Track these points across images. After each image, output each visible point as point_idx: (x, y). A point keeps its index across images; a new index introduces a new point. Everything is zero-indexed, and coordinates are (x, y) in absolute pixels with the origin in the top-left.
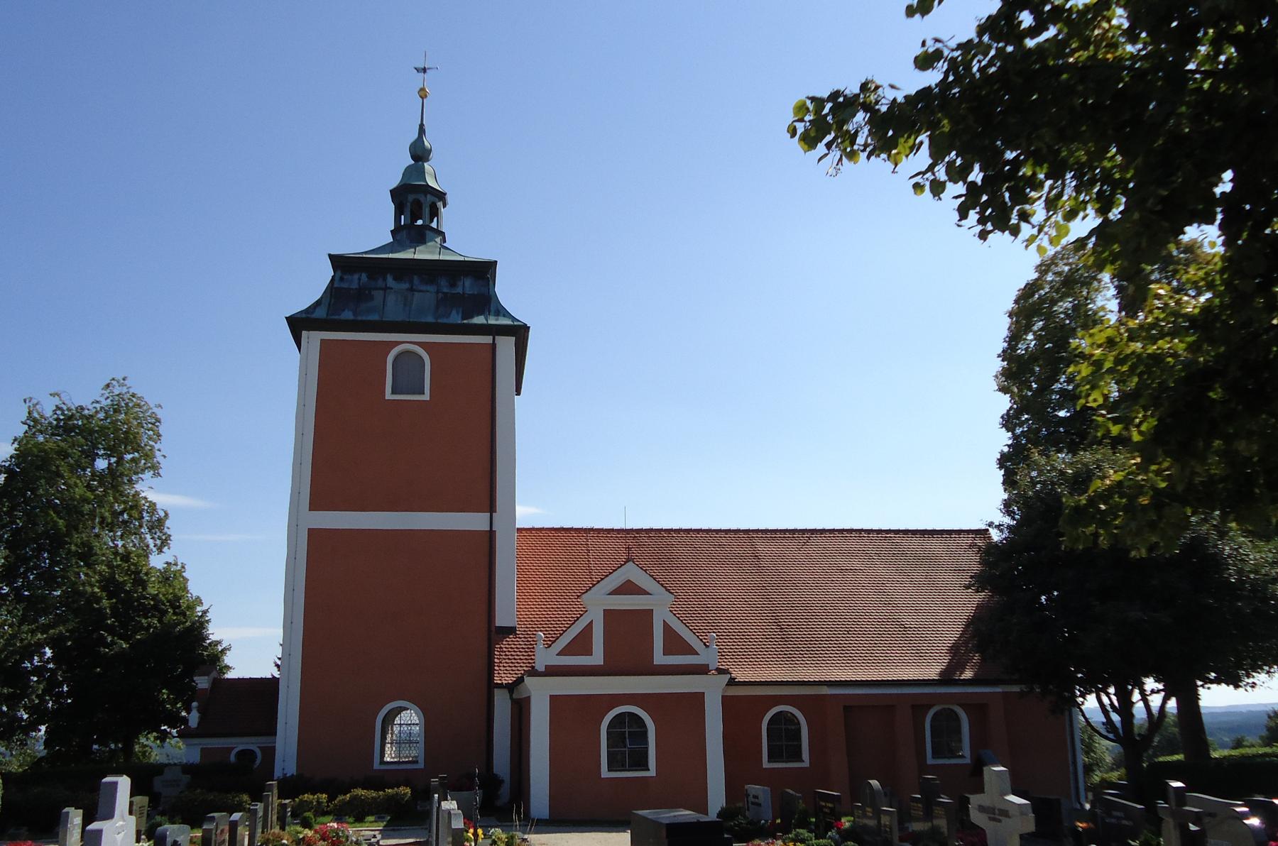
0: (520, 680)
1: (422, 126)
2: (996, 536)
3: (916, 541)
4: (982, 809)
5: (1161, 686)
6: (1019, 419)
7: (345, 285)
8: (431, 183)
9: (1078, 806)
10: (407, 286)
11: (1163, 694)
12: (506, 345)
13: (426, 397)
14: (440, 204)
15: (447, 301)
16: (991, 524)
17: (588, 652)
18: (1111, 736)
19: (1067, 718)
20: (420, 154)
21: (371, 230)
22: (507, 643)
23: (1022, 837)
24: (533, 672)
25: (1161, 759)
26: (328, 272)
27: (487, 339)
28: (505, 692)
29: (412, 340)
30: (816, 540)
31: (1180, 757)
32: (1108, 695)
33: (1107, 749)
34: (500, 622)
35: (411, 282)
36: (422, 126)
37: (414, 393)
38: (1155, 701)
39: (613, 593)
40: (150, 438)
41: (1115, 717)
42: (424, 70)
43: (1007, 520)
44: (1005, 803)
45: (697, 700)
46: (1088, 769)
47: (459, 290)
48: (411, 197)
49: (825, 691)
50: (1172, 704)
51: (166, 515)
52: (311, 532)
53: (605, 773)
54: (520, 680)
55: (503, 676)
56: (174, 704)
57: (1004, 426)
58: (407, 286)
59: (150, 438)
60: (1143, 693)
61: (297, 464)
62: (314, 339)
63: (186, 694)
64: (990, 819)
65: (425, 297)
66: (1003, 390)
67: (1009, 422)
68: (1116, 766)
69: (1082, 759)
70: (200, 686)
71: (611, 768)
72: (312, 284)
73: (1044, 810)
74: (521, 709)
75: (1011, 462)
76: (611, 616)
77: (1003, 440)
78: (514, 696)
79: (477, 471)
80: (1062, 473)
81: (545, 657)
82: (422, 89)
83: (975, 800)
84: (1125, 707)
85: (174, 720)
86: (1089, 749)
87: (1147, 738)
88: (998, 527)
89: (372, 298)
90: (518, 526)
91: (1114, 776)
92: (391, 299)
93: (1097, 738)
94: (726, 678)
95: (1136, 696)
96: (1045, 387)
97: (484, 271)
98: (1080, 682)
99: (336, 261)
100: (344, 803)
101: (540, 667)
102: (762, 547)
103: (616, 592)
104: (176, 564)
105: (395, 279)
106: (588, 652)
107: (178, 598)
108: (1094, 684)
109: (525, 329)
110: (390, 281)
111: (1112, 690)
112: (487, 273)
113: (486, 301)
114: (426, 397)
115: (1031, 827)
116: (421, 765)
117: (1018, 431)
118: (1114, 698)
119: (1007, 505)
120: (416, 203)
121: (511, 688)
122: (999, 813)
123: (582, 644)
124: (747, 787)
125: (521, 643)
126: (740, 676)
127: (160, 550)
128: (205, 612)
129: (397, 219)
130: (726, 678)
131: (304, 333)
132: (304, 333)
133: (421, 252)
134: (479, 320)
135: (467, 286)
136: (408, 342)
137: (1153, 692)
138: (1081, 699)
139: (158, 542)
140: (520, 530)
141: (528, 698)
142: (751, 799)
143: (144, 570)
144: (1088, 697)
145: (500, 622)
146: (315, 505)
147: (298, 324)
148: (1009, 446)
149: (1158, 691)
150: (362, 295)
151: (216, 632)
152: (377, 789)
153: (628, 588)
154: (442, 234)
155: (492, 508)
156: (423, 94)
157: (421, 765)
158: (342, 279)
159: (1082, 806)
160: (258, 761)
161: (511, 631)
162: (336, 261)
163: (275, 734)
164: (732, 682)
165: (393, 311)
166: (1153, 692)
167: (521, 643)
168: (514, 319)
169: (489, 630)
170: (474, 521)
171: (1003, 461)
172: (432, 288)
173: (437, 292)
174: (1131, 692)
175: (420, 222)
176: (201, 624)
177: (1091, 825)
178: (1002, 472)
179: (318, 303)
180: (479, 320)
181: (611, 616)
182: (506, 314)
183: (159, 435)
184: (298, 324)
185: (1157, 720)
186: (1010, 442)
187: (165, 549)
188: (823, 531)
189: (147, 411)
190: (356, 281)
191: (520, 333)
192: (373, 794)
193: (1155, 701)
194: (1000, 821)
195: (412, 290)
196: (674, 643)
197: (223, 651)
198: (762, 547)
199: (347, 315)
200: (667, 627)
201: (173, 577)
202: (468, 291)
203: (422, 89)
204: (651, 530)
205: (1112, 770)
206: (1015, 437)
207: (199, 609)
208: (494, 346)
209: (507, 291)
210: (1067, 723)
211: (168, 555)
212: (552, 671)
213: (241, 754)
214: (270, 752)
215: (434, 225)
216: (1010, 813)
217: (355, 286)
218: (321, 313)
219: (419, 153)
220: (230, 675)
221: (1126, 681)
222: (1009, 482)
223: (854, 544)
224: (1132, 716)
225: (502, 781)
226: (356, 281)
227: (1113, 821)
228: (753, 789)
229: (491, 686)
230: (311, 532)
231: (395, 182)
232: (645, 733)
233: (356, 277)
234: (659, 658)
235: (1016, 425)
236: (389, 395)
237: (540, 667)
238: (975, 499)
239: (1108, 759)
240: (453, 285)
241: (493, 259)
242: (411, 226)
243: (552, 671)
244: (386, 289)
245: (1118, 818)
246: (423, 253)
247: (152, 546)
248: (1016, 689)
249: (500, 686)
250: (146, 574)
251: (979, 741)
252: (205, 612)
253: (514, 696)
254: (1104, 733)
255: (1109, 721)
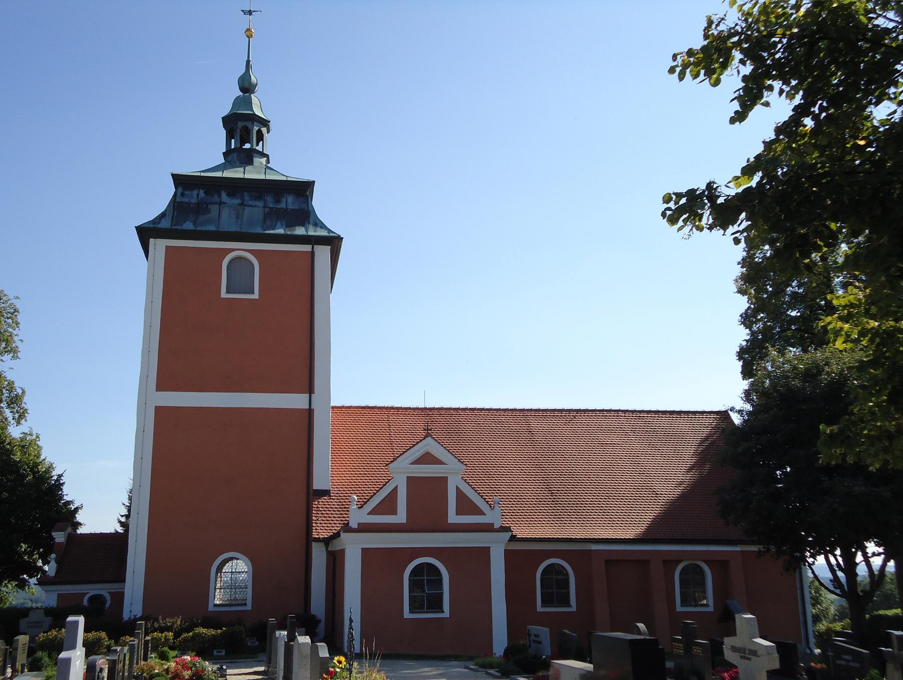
0: (337, 535)
1: (248, 62)
2: (737, 419)
3: (665, 420)
4: (734, 649)
5: (881, 550)
6: (755, 317)
7: (186, 200)
8: (258, 112)
9: (808, 651)
10: (239, 201)
11: (883, 556)
12: (323, 253)
13: (256, 296)
14: (264, 130)
15: (275, 216)
16: (732, 409)
17: (394, 512)
18: (838, 591)
19: (797, 575)
20: (247, 87)
21: (206, 154)
22: (319, 504)
23: (768, 672)
24: (347, 528)
25: (881, 612)
26: (169, 190)
27: (307, 248)
28: (322, 545)
29: (241, 249)
30: (583, 419)
31: (898, 611)
32: (835, 556)
33: (831, 601)
34: (317, 485)
35: (243, 199)
36: (248, 62)
37: (245, 293)
38: (877, 562)
39: (442, 463)
40: (10, 326)
41: (840, 574)
42: (250, 13)
43: (748, 407)
44: (752, 643)
45: (484, 553)
46: (816, 619)
47: (283, 205)
48: (240, 124)
49: (594, 547)
50: (891, 564)
51: (24, 392)
52: (158, 410)
53: (407, 614)
54: (337, 535)
55: (320, 531)
56: (31, 554)
57: (743, 323)
58: (239, 201)
59: (10, 326)
60: (865, 555)
61: (146, 352)
62: (159, 246)
63: (48, 548)
64: (742, 657)
65: (255, 210)
66: (741, 292)
67: (747, 319)
68: (841, 616)
69: (811, 611)
70: (57, 540)
71: (411, 611)
72: (157, 199)
73: (786, 651)
74: (335, 561)
75: (750, 357)
76: (412, 481)
77: (742, 335)
78: (329, 549)
79: (297, 355)
80: (795, 368)
81: (357, 517)
82: (248, 30)
83: (728, 641)
84: (850, 567)
85: (33, 570)
86: (816, 601)
87: (868, 595)
88: (740, 412)
89: (209, 211)
90: (333, 403)
91: (838, 627)
92: (225, 212)
93: (823, 591)
94: (508, 535)
95: (859, 558)
96: (779, 291)
97: (304, 189)
98: (812, 545)
99: (178, 179)
100: (186, 640)
101: (354, 525)
102: (535, 424)
103: (418, 462)
104: (31, 435)
105: (228, 195)
106: (394, 512)
107: (36, 465)
108: (823, 547)
109: (339, 239)
110: (224, 197)
111: (838, 552)
112: (305, 191)
113: (306, 215)
114: (256, 296)
115: (776, 665)
116: (249, 607)
117: (755, 328)
118: (840, 559)
119: (747, 395)
120: (243, 128)
121: (327, 541)
122: (750, 653)
123: (388, 505)
124: (529, 627)
125: (335, 503)
126: (520, 533)
127: (18, 423)
128: (60, 476)
129: (228, 143)
130: (508, 535)
131: (152, 241)
132: (152, 241)
133: (250, 172)
134: (300, 231)
135: (290, 202)
136: (240, 249)
137: (874, 554)
138: (810, 560)
139: (17, 416)
140: (333, 407)
141: (343, 551)
142: (532, 638)
143: (8, 441)
144: (818, 558)
145: (317, 485)
146: (160, 387)
147: (146, 233)
148: (747, 341)
149: (879, 554)
150: (200, 209)
151: (69, 493)
152: (216, 628)
153: (427, 459)
154: (267, 156)
155: (310, 390)
156: (249, 34)
157: (249, 607)
158: (183, 195)
159: (811, 651)
160: (108, 605)
161: (326, 493)
162: (178, 179)
163: (124, 581)
164: (513, 538)
165: (228, 223)
166: (874, 554)
167: (335, 503)
168: (330, 231)
169: (308, 493)
170: (296, 401)
171: (741, 354)
172: (260, 204)
173: (264, 207)
174: (855, 554)
175: (247, 146)
176: (59, 485)
177: (824, 666)
178: (741, 363)
179: (163, 215)
180: (300, 231)
181: (412, 481)
182: (323, 226)
183: (17, 323)
184: (146, 233)
185: (877, 578)
186: (748, 338)
187: (23, 421)
188: (586, 411)
189: (6, 302)
190: (194, 196)
191: (334, 242)
192: (212, 632)
193: (877, 562)
194: (750, 659)
195: (242, 204)
196: (465, 505)
197: (76, 510)
198: (535, 424)
199: (188, 226)
200: (459, 492)
201: (28, 445)
202: (290, 207)
203: (248, 30)
204: (442, 409)
205: (834, 621)
206: (753, 334)
207: (54, 473)
208: (312, 253)
209: (322, 204)
210: (798, 581)
211: (24, 427)
212: (364, 528)
213: (93, 599)
214: (119, 598)
215: (259, 148)
216: (759, 654)
217: (194, 200)
218: (165, 224)
219: (247, 85)
220: (81, 531)
221: (851, 544)
222: (747, 372)
223: (613, 421)
224: (857, 575)
225: (320, 621)
226: (195, 197)
227: (843, 663)
228: (534, 629)
229: (309, 540)
230: (158, 410)
231: (226, 110)
232: (440, 581)
233: (195, 193)
234: (453, 518)
235: (752, 323)
236: (224, 294)
237: (354, 525)
238: (724, 390)
239: (832, 610)
240: (278, 201)
241: (312, 179)
242: (239, 150)
243: (364, 528)
244: (221, 203)
245: (847, 660)
246: (252, 173)
247: (10, 419)
248: (754, 548)
249: (318, 540)
250: (9, 444)
251: (723, 592)
252: (60, 476)
253: (329, 549)
254: (832, 589)
255: (836, 579)
